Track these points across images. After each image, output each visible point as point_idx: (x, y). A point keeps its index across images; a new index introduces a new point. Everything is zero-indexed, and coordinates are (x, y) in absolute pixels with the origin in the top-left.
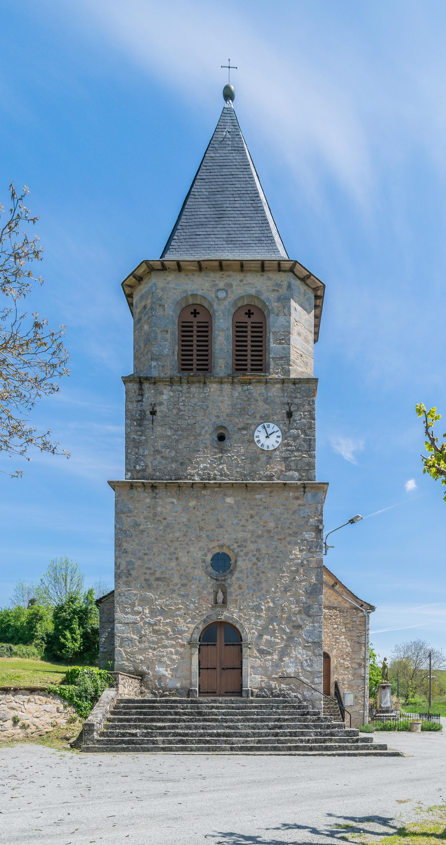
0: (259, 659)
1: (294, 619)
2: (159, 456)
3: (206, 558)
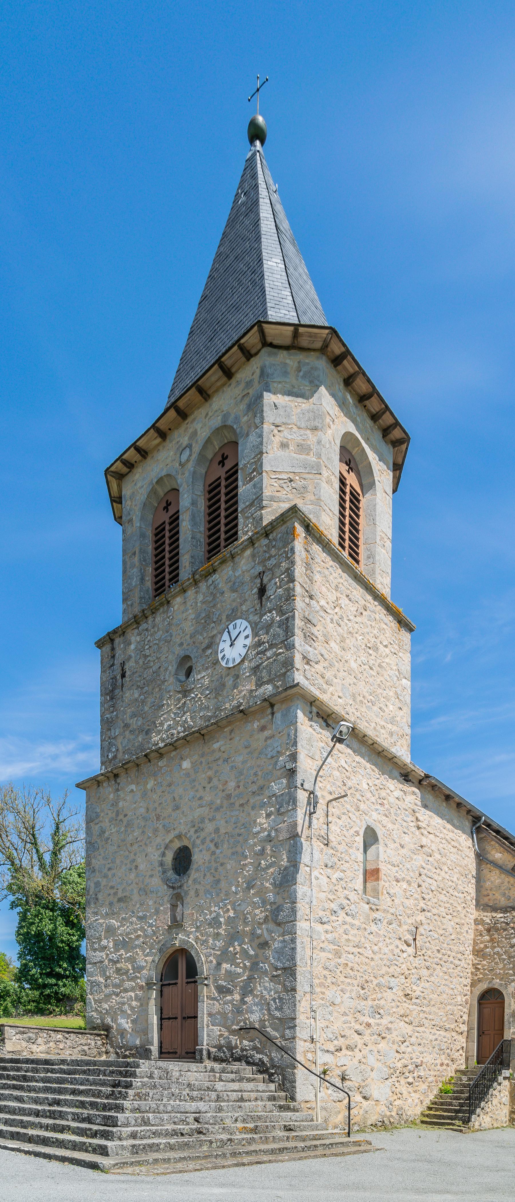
0: (218, 1001)
1: (259, 932)
2: (128, 732)
3: (164, 859)
